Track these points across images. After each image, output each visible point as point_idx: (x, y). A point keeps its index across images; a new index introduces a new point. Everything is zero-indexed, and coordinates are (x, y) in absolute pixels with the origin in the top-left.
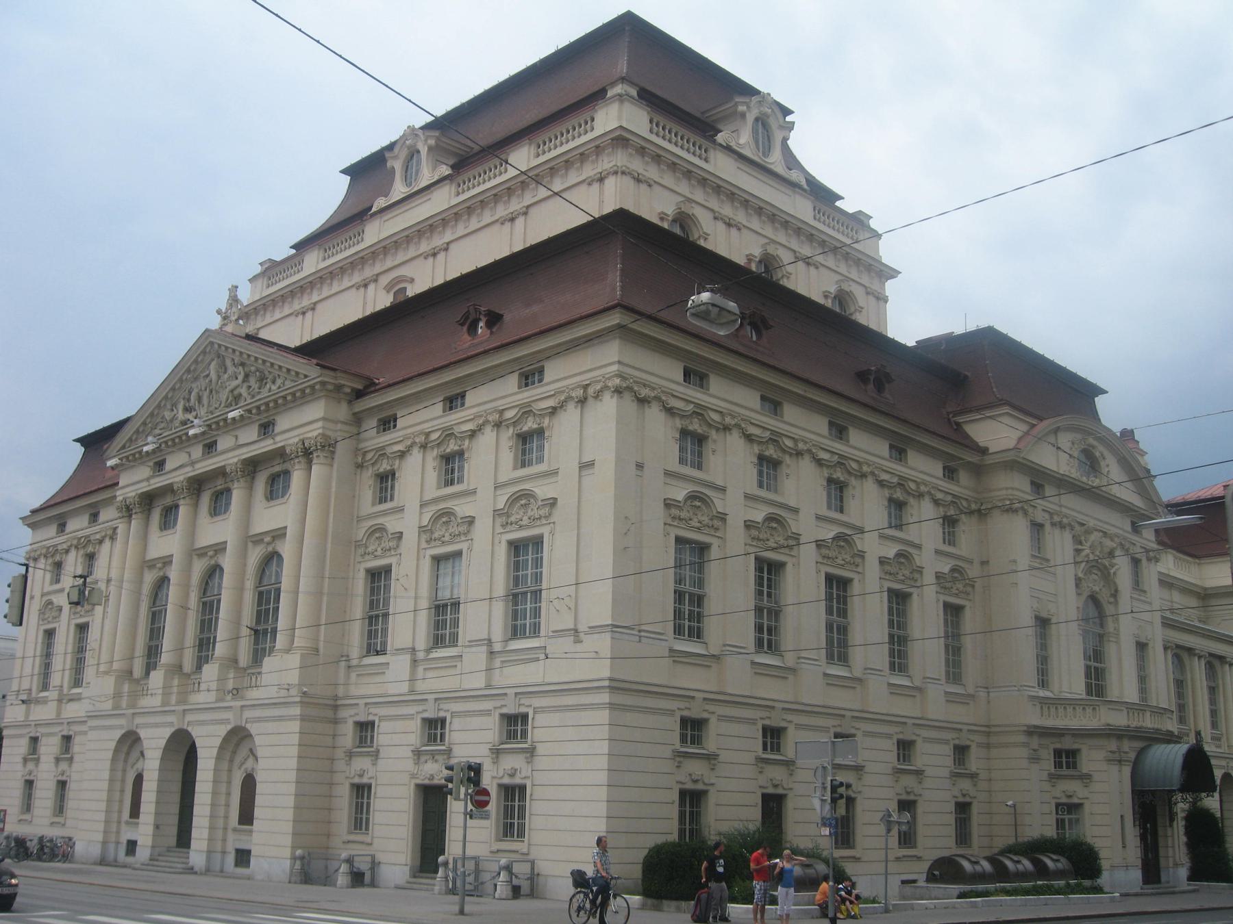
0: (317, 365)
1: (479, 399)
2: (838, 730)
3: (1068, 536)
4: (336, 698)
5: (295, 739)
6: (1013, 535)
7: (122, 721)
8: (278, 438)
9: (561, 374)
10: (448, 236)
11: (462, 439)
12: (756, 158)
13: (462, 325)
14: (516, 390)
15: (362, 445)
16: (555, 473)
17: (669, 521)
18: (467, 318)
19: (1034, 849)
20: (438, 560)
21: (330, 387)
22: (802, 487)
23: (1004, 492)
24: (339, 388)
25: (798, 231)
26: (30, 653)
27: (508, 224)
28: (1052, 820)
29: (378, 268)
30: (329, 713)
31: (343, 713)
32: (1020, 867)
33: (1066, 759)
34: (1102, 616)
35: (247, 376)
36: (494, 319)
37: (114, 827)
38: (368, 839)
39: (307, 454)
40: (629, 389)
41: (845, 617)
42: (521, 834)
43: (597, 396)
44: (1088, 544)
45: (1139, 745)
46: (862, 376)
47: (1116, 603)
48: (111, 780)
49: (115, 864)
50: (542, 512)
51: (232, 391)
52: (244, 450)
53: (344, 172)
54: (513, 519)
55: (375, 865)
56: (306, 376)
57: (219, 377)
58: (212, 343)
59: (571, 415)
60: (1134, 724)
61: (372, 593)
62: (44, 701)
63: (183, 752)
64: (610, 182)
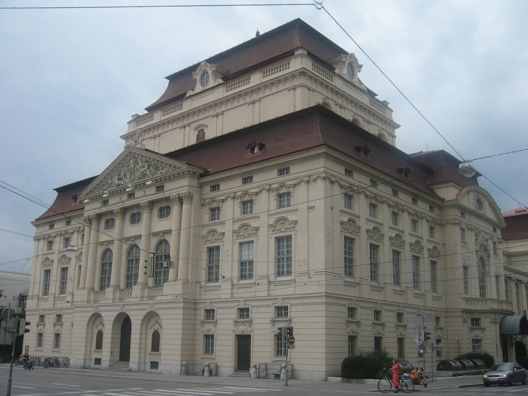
0: (186, 163)
1: (259, 179)
2: (418, 313)
3: (473, 233)
4: (196, 300)
5: (181, 316)
6: (454, 233)
7: (92, 309)
8: (166, 193)
9: (297, 171)
10: (223, 108)
11: (252, 195)
12: (349, 80)
13: (248, 148)
14: (276, 176)
15: (203, 196)
16: (297, 210)
17: (342, 230)
18: (250, 146)
19: (470, 357)
20: (241, 244)
21: (191, 173)
22: (384, 215)
23: (452, 217)
24: (194, 173)
25: (365, 110)
26: (38, 280)
27: (251, 105)
28: (471, 346)
29: (190, 120)
30: (193, 306)
31: (198, 306)
32: (469, 364)
33: (476, 322)
34: (484, 265)
35: (149, 166)
36: (262, 147)
37: (88, 353)
38: (213, 357)
39: (181, 200)
40: (328, 177)
41: (398, 267)
42: (212, 352)
43: (315, 180)
44: (480, 237)
45: (501, 316)
46: (400, 171)
47: (489, 260)
48: (87, 334)
49: (89, 368)
50: (291, 226)
51: (142, 173)
52: (149, 197)
53: (167, 78)
54: (277, 228)
55: (217, 367)
56: (179, 168)
57: (135, 166)
58: (131, 152)
59: (303, 187)
60: (500, 308)
61: (210, 257)
62: (47, 300)
63: (124, 324)
64: (299, 90)
